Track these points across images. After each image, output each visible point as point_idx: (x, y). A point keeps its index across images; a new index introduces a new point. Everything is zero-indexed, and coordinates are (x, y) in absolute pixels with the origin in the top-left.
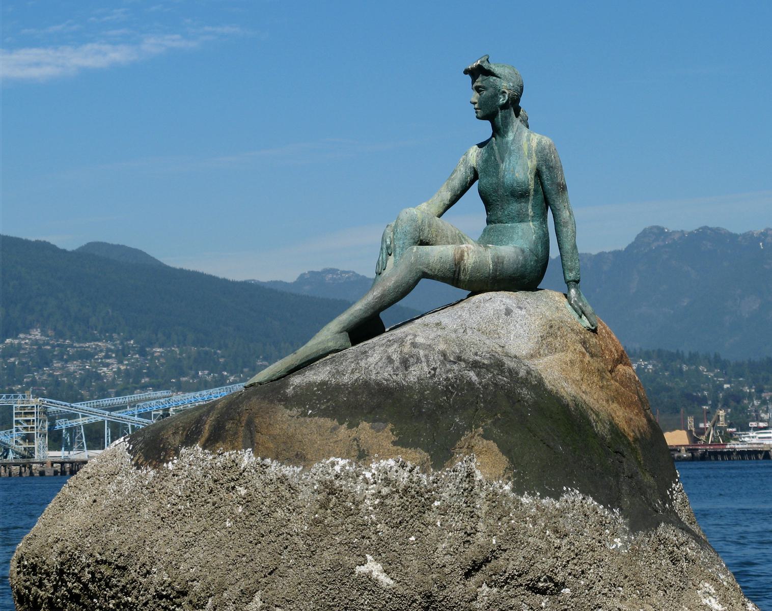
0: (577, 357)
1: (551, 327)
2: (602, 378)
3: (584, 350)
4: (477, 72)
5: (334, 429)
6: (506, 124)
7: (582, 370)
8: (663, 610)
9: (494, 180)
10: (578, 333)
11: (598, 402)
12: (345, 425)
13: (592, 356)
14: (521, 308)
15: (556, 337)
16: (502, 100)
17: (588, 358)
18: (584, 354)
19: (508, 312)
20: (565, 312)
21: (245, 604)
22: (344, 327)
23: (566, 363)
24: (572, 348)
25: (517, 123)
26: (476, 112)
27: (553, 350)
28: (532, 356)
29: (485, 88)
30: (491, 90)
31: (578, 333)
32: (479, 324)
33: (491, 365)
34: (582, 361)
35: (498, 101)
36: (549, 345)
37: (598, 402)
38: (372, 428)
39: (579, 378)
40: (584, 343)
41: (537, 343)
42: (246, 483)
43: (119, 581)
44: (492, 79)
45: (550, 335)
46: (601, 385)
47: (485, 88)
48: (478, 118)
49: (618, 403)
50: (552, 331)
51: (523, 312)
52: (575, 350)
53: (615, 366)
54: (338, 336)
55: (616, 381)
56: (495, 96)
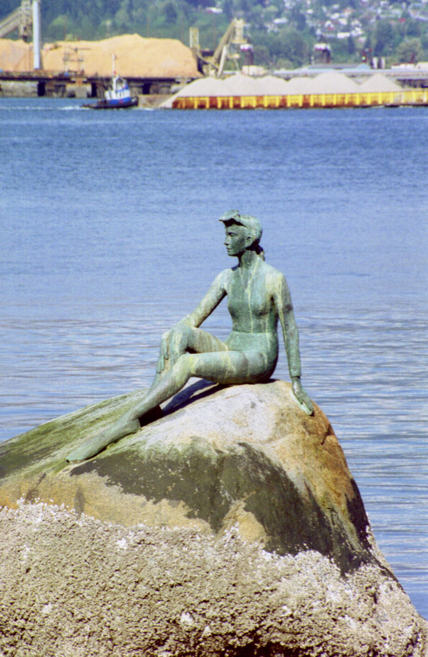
0: (301, 436)
2: (317, 449)
3: (304, 430)
4: (229, 223)
6: (250, 260)
7: (305, 446)
8: (227, 655)
9: (241, 301)
11: (315, 470)
12: (151, 501)
13: (310, 433)
14: (261, 401)
15: (286, 422)
16: (248, 244)
17: (307, 436)
18: (304, 433)
19: (253, 406)
20: (290, 401)
22: (137, 416)
24: (296, 430)
25: (258, 258)
26: (229, 251)
27: (284, 433)
28: (270, 440)
30: (240, 236)
32: (234, 416)
33: (363, 542)
34: (304, 440)
35: (244, 244)
37: (315, 470)
39: (302, 453)
40: (304, 424)
41: (274, 429)
43: (145, 608)
44: (241, 227)
45: (283, 421)
46: (316, 455)
48: (230, 255)
49: (328, 468)
50: (283, 418)
51: (263, 405)
52: (299, 431)
53: (324, 439)
54: (132, 422)
55: (326, 450)
56: (242, 241)
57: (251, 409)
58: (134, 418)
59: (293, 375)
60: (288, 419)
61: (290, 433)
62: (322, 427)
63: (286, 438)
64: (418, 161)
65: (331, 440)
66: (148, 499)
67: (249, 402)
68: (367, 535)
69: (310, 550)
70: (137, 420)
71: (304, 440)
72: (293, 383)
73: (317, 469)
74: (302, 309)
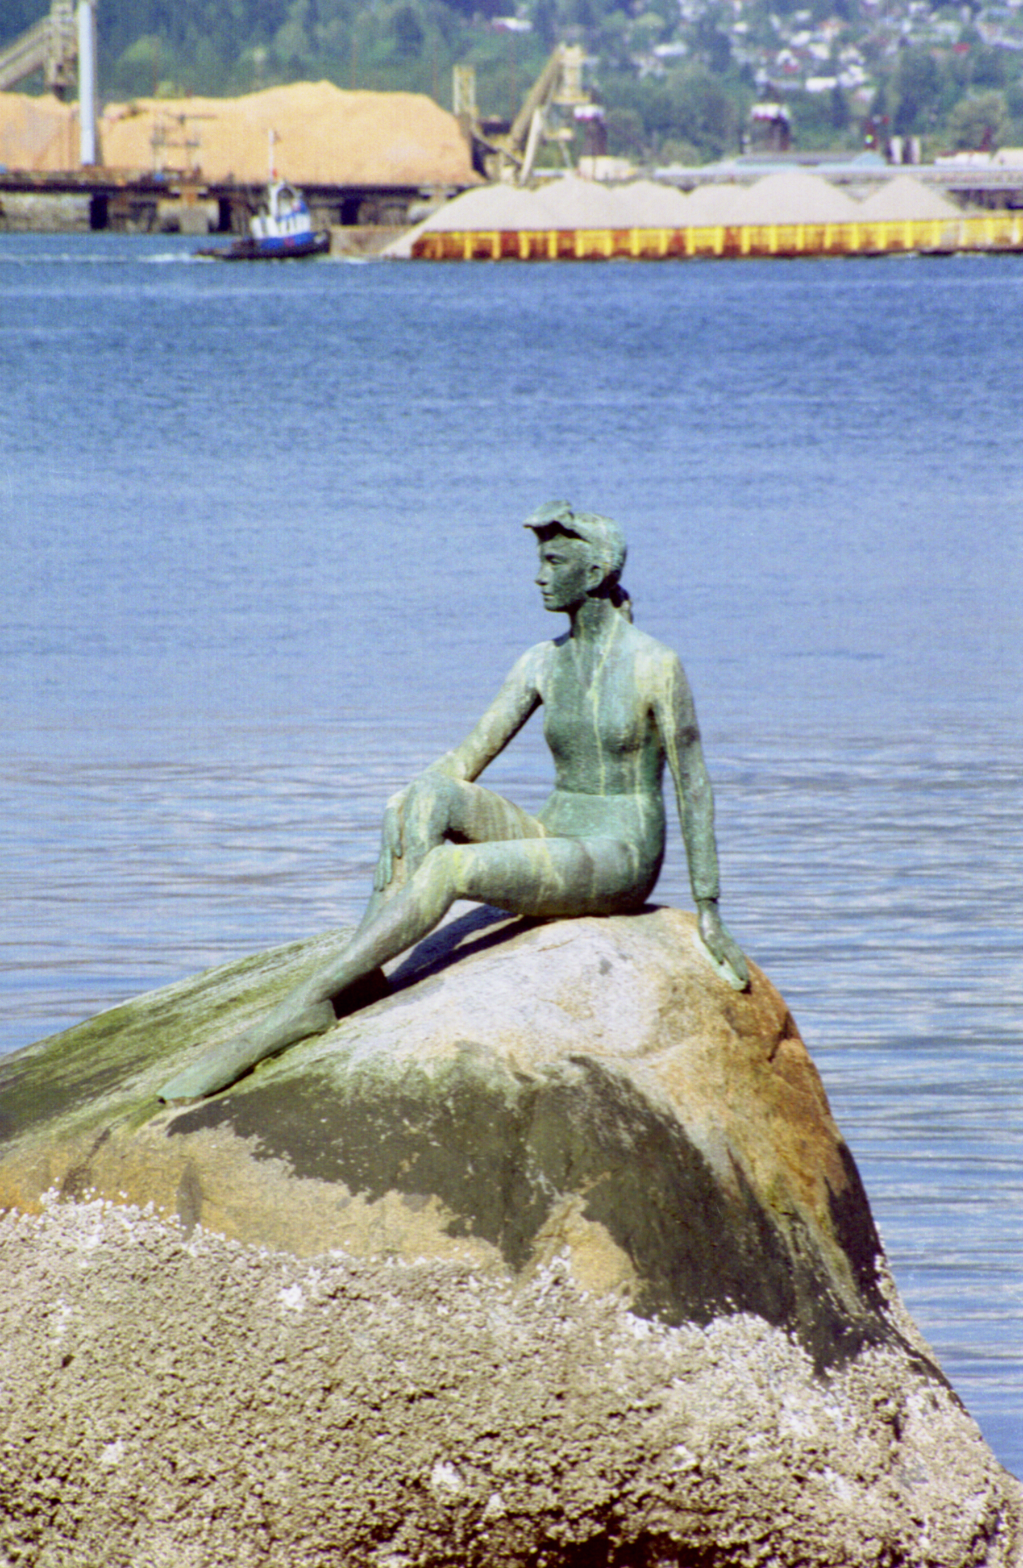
1: (675, 990)
2: (757, 1072)
3: (727, 1026)
4: (548, 532)
5: (343, 1204)
6: (598, 620)
7: (729, 1064)
9: (575, 718)
10: (717, 994)
12: (361, 1197)
13: (741, 1033)
14: (624, 957)
16: (592, 582)
17: (735, 1041)
19: (606, 968)
21: (645, 1414)
22: (327, 992)
23: (701, 1058)
25: (616, 616)
27: (679, 1034)
28: (646, 1050)
29: (564, 560)
30: (573, 562)
31: (717, 994)
32: (560, 993)
35: (584, 583)
36: (672, 1024)
37: (753, 1122)
38: (404, 1203)
39: (721, 1081)
40: (727, 1012)
41: (654, 1023)
42: (553, 1381)
44: (576, 543)
45: (677, 1004)
46: (756, 1086)
47: (564, 560)
48: (549, 609)
49: (784, 1116)
50: (676, 997)
51: (629, 966)
52: (714, 1028)
54: (315, 1007)
55: (779, 1073)
57: (599, 976)
58: (320, 997)
59: (700, 894)
60: (688, 1000)
61: (693, 1034)
62: (769, 1020)
63: (684, 1046)
64: (998, 384)
65: (791, 1051)
66: (354, 1191)
67: (596, 960)
68: (877, 1276)
69: (740, 1312)
70: (328, 1002)
71: (726, 1049)
72: (701, 915)
73: (757, 1120)
74: (722, 738)
